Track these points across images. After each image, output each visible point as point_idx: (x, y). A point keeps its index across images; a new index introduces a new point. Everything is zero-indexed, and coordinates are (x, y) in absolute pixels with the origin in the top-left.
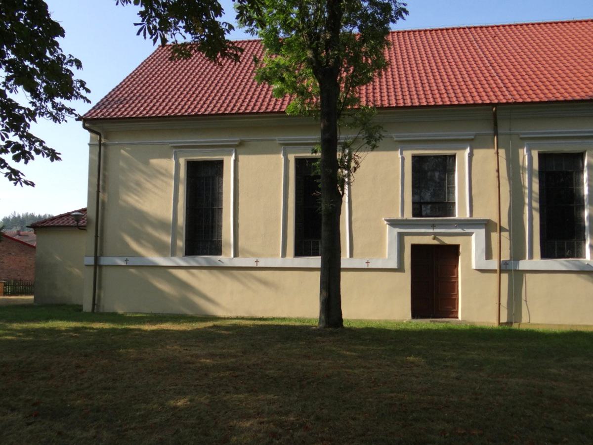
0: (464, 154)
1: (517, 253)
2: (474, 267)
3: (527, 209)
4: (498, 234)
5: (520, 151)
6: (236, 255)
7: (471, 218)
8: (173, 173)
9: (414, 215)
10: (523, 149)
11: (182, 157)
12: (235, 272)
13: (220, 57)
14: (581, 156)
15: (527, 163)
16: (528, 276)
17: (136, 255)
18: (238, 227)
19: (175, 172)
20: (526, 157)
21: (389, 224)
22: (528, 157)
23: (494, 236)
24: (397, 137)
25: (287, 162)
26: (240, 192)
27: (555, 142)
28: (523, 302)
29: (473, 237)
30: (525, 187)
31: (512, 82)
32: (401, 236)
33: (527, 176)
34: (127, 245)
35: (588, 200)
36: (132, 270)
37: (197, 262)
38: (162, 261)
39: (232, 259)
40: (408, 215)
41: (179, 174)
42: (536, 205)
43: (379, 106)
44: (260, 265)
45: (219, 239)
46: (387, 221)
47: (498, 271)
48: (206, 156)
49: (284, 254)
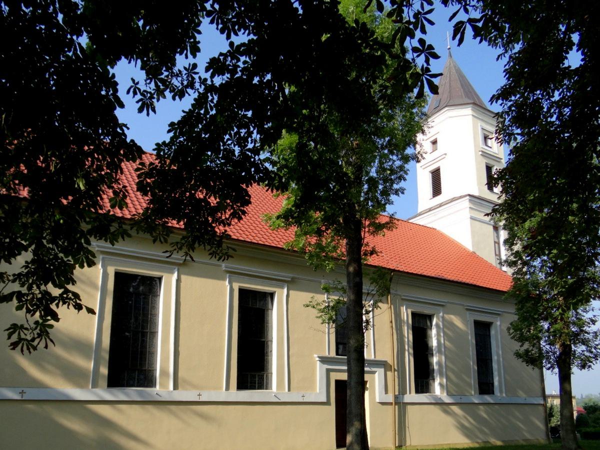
0: (171, 278)
1: (403, 391)
2: (378, 400)
3: (407, 353)
4: (393, 373)
5: (402, 308)
6: (176, 387)
7: (329, 356)
8: (100, 283)
9: (337, 354)
10: (403, 307)
11: (112, 265)
12: (173, 407)
13: (98, 156)
14: (430, 317)
15: (406, 318)
16: (409, 407)
17: (37, 384)
18: (179, 355)
19: (102, 282)
20: (405, 313)
21: (319, 361)
22: (406, 314)
23: (389, 373)
24: (98, 246)
25: (232, 290)
26: (181, 316)
27: (132, 260)
28: (407, 428)
29: (377, 374)
30: (405, 337)
31: (134, 204)
32: (328, 371)
33: (406, 328)
34: (23, 372)
35: (437, 350)
36: (30, 406)
37: (127, 394)
38: (78, 394)
39: (172, 391)
40: (333, 354)
41: (107, 285)
42: (411, 351)
43: (355, 265)
44: (203, 399)
45: (150, 369)
46: (319, 357)
47: (394, 404)
48: (136, 268)
49: (227, 388)
